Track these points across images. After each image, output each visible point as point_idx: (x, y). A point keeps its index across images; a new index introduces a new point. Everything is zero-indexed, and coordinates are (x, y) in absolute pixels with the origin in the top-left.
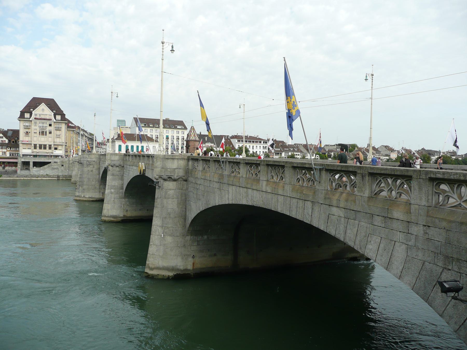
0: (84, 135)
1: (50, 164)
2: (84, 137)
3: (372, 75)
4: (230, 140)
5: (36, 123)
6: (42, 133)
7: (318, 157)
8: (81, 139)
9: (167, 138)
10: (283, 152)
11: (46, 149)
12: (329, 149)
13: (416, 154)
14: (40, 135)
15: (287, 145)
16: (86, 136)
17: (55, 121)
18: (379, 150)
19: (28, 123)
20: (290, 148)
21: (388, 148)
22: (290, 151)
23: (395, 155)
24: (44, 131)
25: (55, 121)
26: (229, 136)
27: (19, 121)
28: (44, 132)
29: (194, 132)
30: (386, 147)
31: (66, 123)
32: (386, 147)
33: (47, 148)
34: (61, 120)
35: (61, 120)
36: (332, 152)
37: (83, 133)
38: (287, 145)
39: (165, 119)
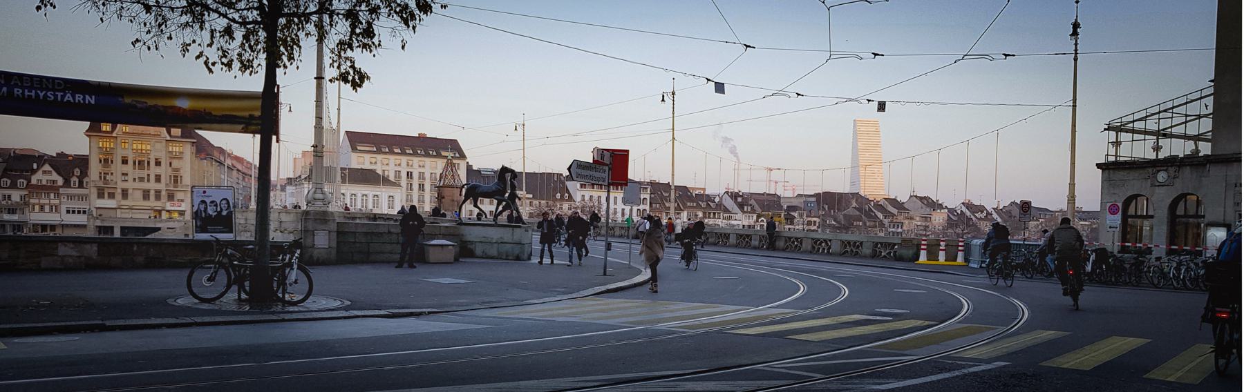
0: (235, 167)
1: (160, 232)
2: (235, 172)
3: (673, 94)
4: (564, 184)
5: (127, 141)
6: (139, 164)
7: (762, 221)
8: (228, 177)
9: (409, 175)
10: (683, 211)
11: (149, 199)
12: (789, 204)
13: (995, 216)
14: (135, 169)
15: (694, 195)
16: (238, 170)
17: (169, 138)
18: (906, 206)
19: (112, 144)
20: (701, 203)
21: (928, 202)
22: (699, 207)
23: (937, 218)
24: (143, 159)
25: (169, 138)
26: (562, 175)
27: (88, 139)
28: (144, 161)
29: (452, 170)
30: (923, 201)
31: (193, 142)
32: (921, 199)
33: (152, 197)
34: (182, 136)
35: (182, 136)
36: (795, 211)
37: (232, 164)
38: (694, 195)
39: (417, 136)
